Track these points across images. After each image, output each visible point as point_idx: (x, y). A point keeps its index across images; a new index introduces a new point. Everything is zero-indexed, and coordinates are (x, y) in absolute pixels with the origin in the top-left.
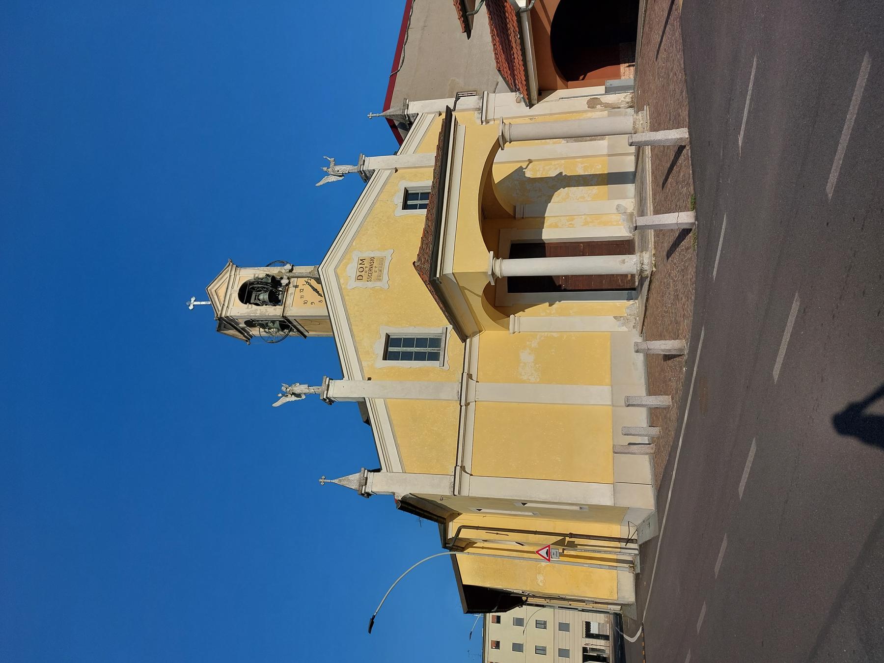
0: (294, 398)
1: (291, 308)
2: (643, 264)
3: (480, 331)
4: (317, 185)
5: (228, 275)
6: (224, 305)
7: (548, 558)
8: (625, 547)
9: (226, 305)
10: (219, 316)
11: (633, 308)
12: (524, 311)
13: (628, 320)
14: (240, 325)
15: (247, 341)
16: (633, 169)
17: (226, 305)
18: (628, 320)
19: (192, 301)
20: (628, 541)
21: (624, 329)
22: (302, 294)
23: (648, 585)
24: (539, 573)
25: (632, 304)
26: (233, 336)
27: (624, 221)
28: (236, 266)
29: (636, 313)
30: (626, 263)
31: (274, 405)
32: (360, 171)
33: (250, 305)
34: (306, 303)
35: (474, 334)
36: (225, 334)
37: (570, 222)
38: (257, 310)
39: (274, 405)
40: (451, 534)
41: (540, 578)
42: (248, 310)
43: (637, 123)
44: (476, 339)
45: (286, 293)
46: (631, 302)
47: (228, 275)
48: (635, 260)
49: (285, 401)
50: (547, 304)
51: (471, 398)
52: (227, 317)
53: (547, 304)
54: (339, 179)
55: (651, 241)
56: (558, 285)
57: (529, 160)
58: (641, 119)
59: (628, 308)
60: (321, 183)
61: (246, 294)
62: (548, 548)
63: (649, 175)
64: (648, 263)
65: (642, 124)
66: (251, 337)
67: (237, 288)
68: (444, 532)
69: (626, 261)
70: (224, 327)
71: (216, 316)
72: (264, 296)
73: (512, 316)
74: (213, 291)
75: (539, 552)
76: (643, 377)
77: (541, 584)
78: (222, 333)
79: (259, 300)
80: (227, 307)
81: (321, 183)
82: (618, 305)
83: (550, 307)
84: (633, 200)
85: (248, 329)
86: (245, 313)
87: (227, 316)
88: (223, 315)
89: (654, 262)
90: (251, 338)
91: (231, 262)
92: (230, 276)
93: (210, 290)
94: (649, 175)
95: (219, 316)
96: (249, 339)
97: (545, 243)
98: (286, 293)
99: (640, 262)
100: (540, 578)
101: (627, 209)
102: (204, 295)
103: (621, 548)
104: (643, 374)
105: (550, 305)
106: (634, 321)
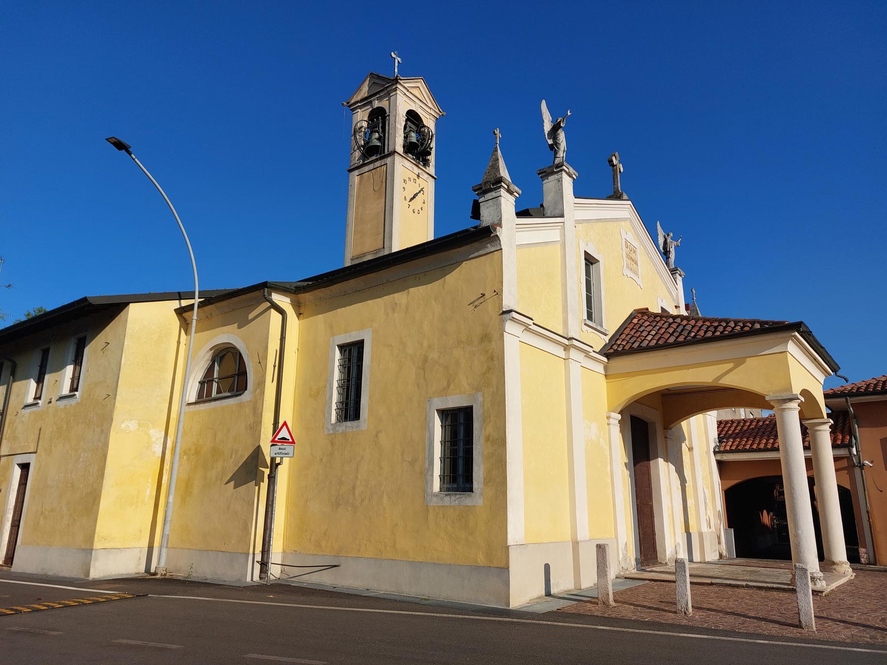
0: (547, 127)
1: (401, 164)
3: (606, 376)
4: (658, 222)
5: (430, 105)
6: (408, 91)
7: (276, 439)
8: (255, 560)
9: (407, 93)
10: (399, 81)
14: (376, 102)
15: (348, 103)
16: (694, 561)
17: (407, 93)
19: (398, 58)
20: (264, 565)
22: (412, 180)
23: (272, 600)
24: (139, 424)
26: (359, 88)
28: (437, 119)
31: (544, 102)
32: (677, 270)
33: (405, 119)
34: (404, 182)
35: (606, 368)
36: (364, 81)
38: (401, 126)
39: (544, 102)
40: (277, 298)
41: (132, 425)
42: (401, 116)
44: (600, 369)
45: (415, 163)
47: (430, 105)
49: (544, 117)
51: (573, 353)
52: (395, 89)
54: (660, 247)
57: (693, 448)
60: (659, 227)
61: (413, 117)
62: (291, 440)
66: (353, 110)
67: (420, 112)
68: (283, 289)
70: (374, 83)
71: (401, 78)
72: (413, 137)
73: (619, 417)
74: (419, 85)
75: (285, 426)
77: (123, 425)
78: (366, 79)
79: (410, 131)
80: (405, 94)
81: (659, 227)
85: (369, 109)
86: (398, 111)
87: (396, 90)
88: (399, 86)
90: (351, 110)
91: (442, 115)
92: (431, 108)
93: (420, 82)
95: (399, 81)
96: (349, 106)
97: (649, 460)
98: (415, 163)
100: (132, 425)
102: (410, 72)
103: (254, 554)
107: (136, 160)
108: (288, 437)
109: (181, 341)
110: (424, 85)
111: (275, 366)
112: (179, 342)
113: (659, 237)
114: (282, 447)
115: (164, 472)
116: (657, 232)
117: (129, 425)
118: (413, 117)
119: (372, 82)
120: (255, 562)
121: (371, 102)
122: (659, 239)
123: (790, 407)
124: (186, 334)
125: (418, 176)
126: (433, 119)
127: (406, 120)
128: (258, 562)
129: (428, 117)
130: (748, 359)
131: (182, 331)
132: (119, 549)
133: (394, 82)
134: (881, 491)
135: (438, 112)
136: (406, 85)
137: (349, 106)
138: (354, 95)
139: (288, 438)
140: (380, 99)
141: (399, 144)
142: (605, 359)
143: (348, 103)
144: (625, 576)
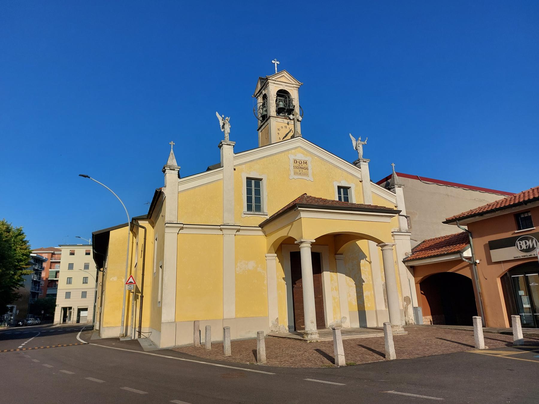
3: (266, 236)
5: (294, 83)
6: (276, 81)
7: (128, 283)
8: (136, 330)
9: (276, 82)
10: (268, 78)
11: (284, 330)
12: (279, 262)
13: (276, 326)
14: (263, 91)
15: (254, 95)
16: (368, 326)
17: (276, 82)
18: (276, 326)
19: (277, 62)
23: (113, 346)
24: (118, 278)
30: (311, 324)
33: (276, 96)
35: (264, 232)
40: (141, 223)
41: (115, 279)
42: (273, 96)
44: (261, 233)
45: (284, 118)
46: (287, 328)
47: (294, 83)
49: (219, 119)
50: (284, 276)
51: (225, 232)
53: (284, 276)
56: (296, 282)
57: (371, 262)
61: (282, 94)
62: (134, 283)
65: (396, 330)
66: (257, 98)
68: (142, 218)
69: (313, 324)
70: (262, 82)
79: (279, 102)
80: (274, 83)
83: (282, 278)
85: (262, 96)
88: (269, 81)
90: (256, 98)
96: (255, 97)
97: (321, 273)
100: (115, 279)
103: (135, 328)
107: (93, 179)
108: (133, 281)
109: (134, 241)
110: (287, 73)
111: (142, 251)
112: (133, 242)
113: (353, 142)
114: (130, 286)
115: (130, 296)
116: (351, 140)
117: (114, 278)
118: (282, 94)
119: (261, 82)
120: (136, 331)
121: (262, 92)
122: (353, 143)
123: (303, 246)
124: (136, 238)
125: (288, 124)
126: (296, 89)
127: (277, 97)
128: (137, 331)
129: (293, 89)
130: (294, 223)
131: (134, 237)
132: (113, 327)
133: (267, 80)
134: (486, 279)
135: (298, 84)
136: (273, 79)
137: (255, 97)
138: (255, 91)
139: (132, 282)
140: (264, 90)
141: (272, 110)
142: (260, 228)
143: (254, 95)
144: (268, 335)
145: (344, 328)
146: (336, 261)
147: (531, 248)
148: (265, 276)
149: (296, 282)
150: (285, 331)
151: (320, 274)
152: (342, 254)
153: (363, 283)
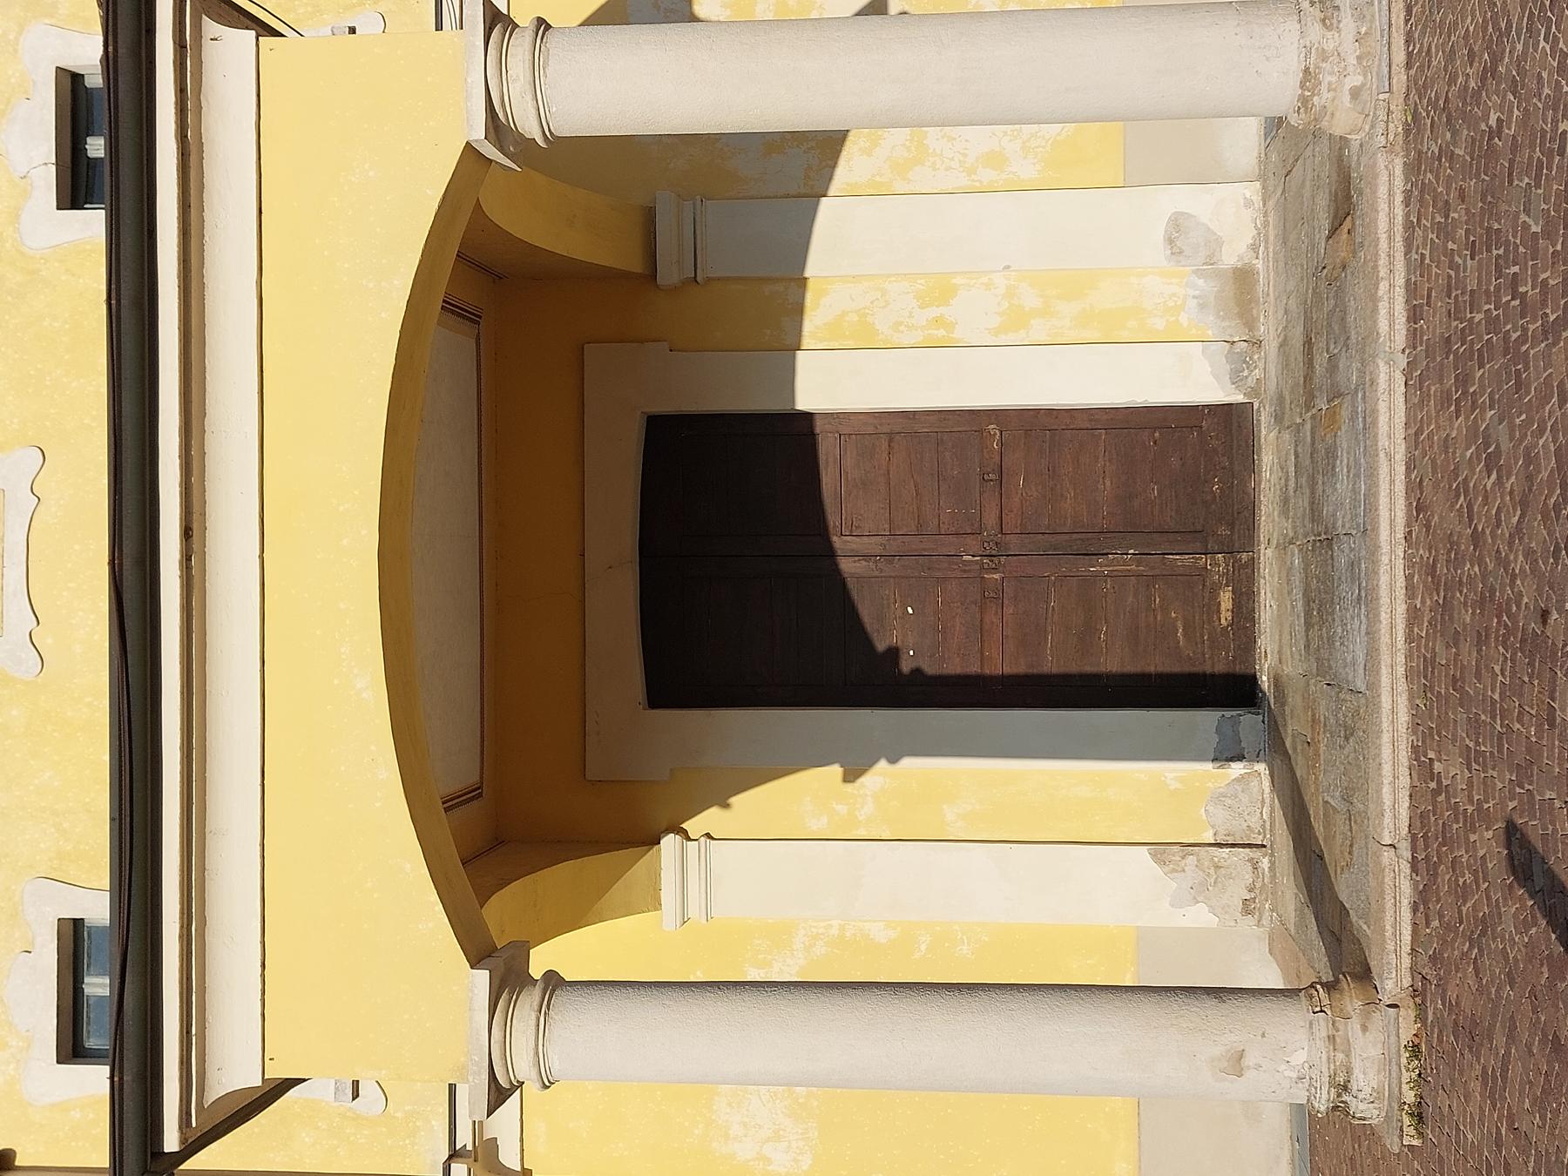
2: (1345, 1088)
11: (1245, 799)
12: (726, 806)
13: (1217, 867)
18: (1217, 867)
21: (1200, 916)
25: (1240, 779)
27: (1202, 307)
29: (1257, 827)
30: (1250, 1075)
37: (933, 312)
43: (1327, 79)
46: (1237, 769)
48: (1300, 1057)
50: (836, 770)
53: (836, 770)
55: (1397, 934)
56: (881, 646)
58: (1352, 60)
59: (1218, 798)
63: (1392, 482)
64: (1378, 1092)
65: (1355, 93)
69: (1249, 1061)
76: (1286, 1156)
82: (1174, 785)
83: (849, 787)
84: (1252, 191)
89: (1410, 1097)
94: (1392, 482)
99: (1332, 1077)
101: (1220, 243)
104: (1287, 1145)
105: (851, 776)
106: (1248, 878)
145: (1254, 248)
146: (709, 280)
147: (204, 16)
148: (835, 931)
149: (881, 646)
150: (1255, 783)
151: (819, 426)
152: (649, 218)
153: (906, 667)
